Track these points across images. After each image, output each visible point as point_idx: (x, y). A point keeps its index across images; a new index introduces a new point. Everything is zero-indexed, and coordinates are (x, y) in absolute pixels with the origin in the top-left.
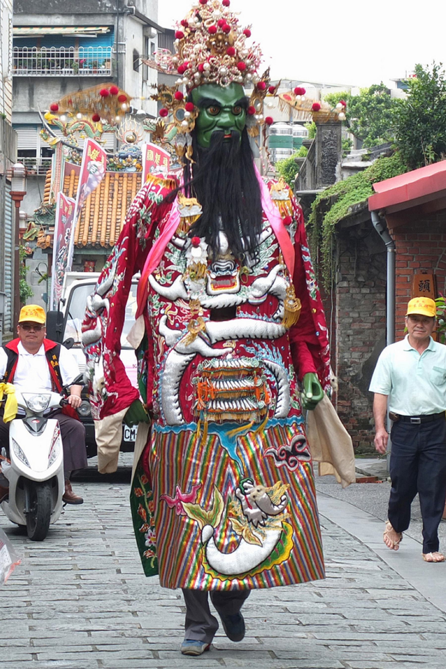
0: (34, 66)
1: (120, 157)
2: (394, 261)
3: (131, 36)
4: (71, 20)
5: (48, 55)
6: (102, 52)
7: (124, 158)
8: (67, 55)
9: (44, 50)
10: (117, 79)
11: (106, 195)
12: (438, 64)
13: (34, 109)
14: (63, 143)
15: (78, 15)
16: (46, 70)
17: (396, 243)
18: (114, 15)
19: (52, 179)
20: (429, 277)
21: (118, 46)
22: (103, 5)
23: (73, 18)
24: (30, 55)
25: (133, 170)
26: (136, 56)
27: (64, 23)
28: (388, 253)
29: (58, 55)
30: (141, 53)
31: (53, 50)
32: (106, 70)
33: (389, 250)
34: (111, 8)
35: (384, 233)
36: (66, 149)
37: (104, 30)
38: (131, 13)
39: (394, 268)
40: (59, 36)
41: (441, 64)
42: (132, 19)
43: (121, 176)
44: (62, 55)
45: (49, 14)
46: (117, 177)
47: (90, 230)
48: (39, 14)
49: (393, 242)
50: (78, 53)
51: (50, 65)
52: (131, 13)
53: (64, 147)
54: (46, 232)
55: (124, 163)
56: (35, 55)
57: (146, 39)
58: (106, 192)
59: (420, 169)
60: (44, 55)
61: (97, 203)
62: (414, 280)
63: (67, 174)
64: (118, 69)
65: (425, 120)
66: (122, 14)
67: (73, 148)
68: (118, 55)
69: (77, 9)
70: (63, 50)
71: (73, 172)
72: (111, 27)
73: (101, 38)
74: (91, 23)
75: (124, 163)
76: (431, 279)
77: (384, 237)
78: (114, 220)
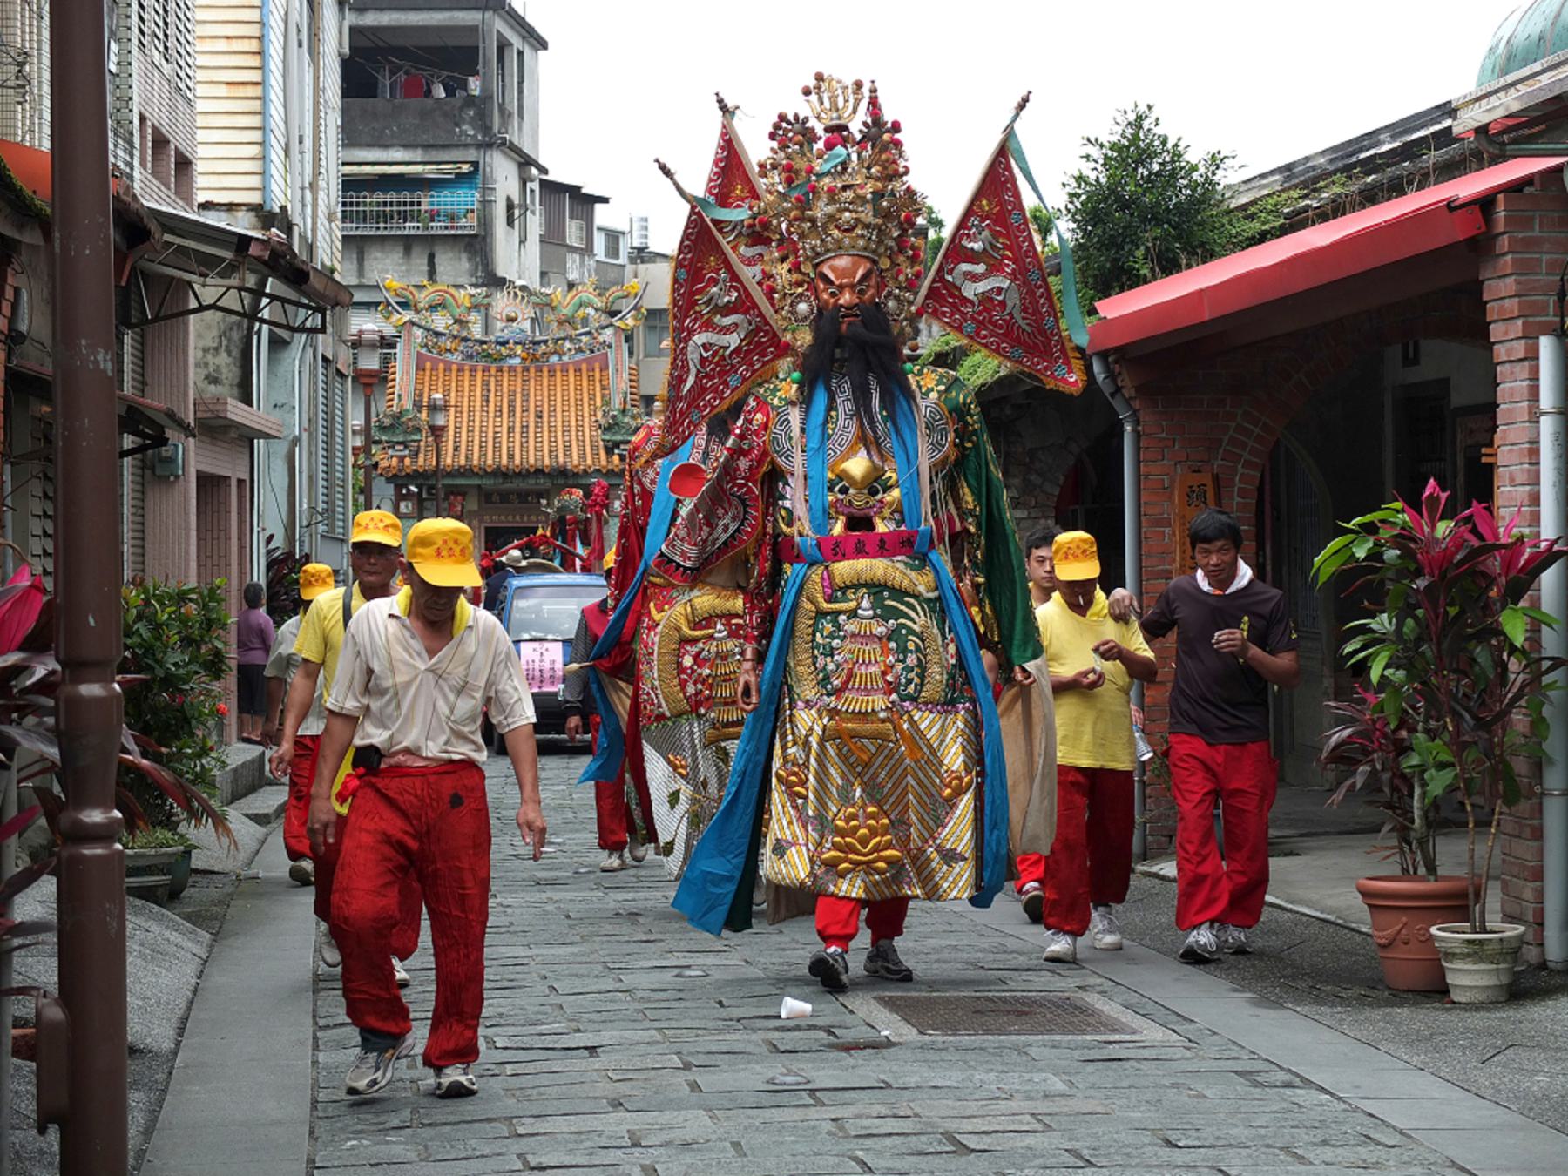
0: (365, 221)
1: (498, 343)
2: (1137, 449)
3: (504, 177)
4: (418, 155)
5: (385, 204)
6: (463, 199)
7: (504, 344)
8: (412, 204)
9: (379, 197)
10: (484, 238)
11: (478, 399)
12: (1142, 108)
13: (364, 281)
14: (413, 324)
15: (427, 147)
16: (382, 225)
17: (1141, 414)
18: (479, 146)
19: (398, 376)
20: (1207, 479)
21: (485, 191)
22: (463, 132)
23: (419, 151)
24: (358, 204)
25: (516, 361)
26: (510, 206)
27: (407, 159)
28: (1126, 435)
29: (399, 204)
30: (516, 202)
31: (392, 197)
32: (468, 225)
33: (1128, 428)
34: (475, 136)
35: (1118, 396)
36: (418, 332)
37: (465, 168)
38: (504, 144)
39: (1137, 462)
40: (401, 176)
41: (1150, 107)
42: (504, 153)
43: (500, 370)
44: (405, 204)
45: (386, 146)
46: (493, 371)
47: (456, 449)
48: (370, 145)
49: (1135, 412)
50: (427, 201)
51: (387, 217)
52: (504, 144)
53: (415, 329)
54: (390, 452)
55: (504, 351)
56: (365, 204)
57: (524, 182)
58: (478, 393)
59: (1202, 267)
60: (378, 204)
61: (465, 409)
62: (1177, 485)
63: (420, 368)
64: (486, 223)
65: (1124, 205)
66: (489, 146)
67: (428, 330)
68: (486, 204)
69: (426, 138)
70: (405, 196)
71: (428, 365)
72: (475, 164)
73: (461, 179)
74: (447, 158)
75: (504, 351)
76: (1208, 481)
77: (1117, 404)
78: (491, 434)
